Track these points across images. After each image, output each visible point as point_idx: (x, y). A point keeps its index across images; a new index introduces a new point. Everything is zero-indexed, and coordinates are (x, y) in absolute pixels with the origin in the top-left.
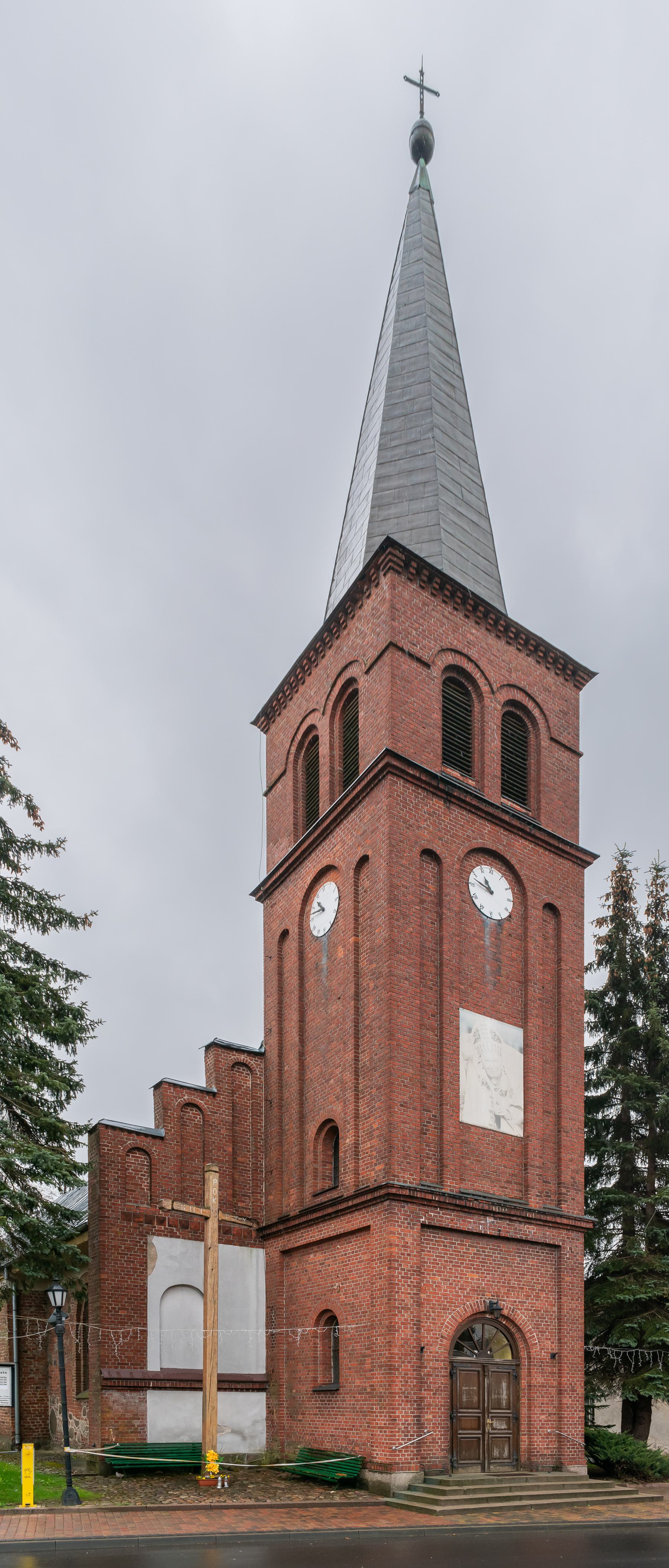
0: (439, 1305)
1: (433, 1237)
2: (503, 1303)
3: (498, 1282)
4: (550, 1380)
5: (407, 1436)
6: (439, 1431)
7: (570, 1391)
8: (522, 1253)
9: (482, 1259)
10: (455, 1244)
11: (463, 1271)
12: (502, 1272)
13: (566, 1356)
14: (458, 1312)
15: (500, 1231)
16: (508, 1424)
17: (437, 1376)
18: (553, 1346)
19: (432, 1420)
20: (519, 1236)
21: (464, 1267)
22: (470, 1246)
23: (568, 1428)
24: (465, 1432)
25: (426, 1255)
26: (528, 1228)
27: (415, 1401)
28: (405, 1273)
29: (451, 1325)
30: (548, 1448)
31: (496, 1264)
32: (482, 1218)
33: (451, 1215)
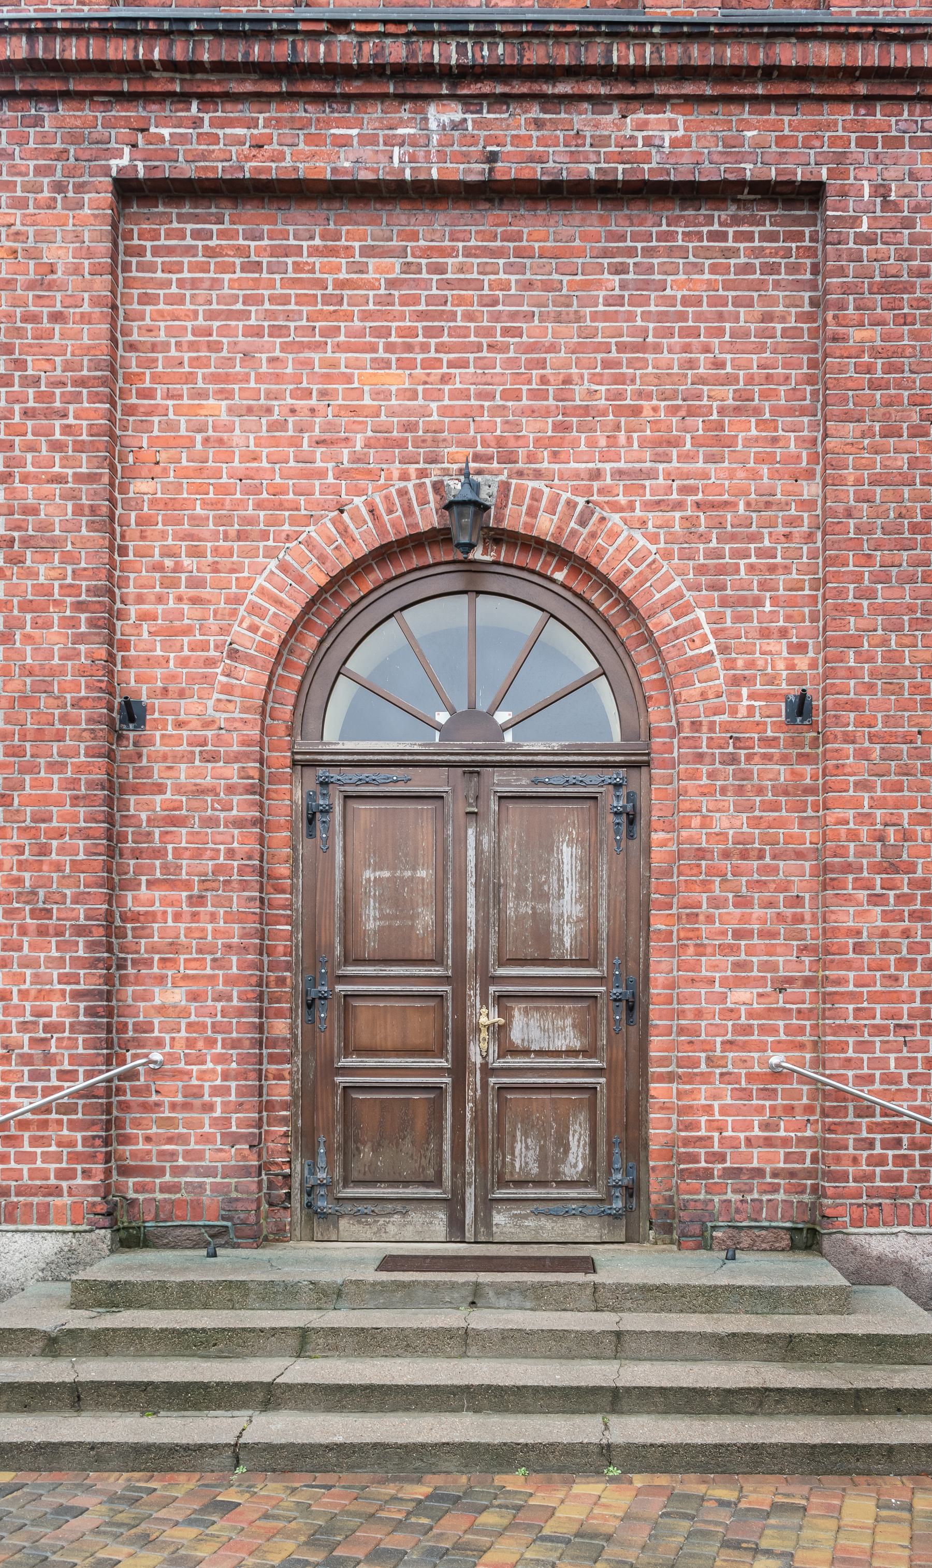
0: (219, 520)
1: (196, 235)
2: (531, 484)
3: (505, 395)
4: (781, 823)
5: (45, 1076)
6: (220, 1059)
7: (877, 868)
8: (631, 252)
9: (430, 300)
10: (298, 251)
11: (334, 365)
12: (531, 348)
13: (856, 706)
14: (309, 543)
15: (492, 158)
16: (587, 1028)
17: (211, 822)
18: (802, 662)
19: (185, 1013)
20: (591, 171)
21: (338, 347)
22: (368, 252)
23: (863, 1046)
24: (371, 1062)
25: (162, 315)
26: (641, 126)
27: (80, 931)
28: (39, 397)
29: (278, 602)
30: (768, 1142)
31: (496, 317)
32: (405, 112)
33: (253, 124)
